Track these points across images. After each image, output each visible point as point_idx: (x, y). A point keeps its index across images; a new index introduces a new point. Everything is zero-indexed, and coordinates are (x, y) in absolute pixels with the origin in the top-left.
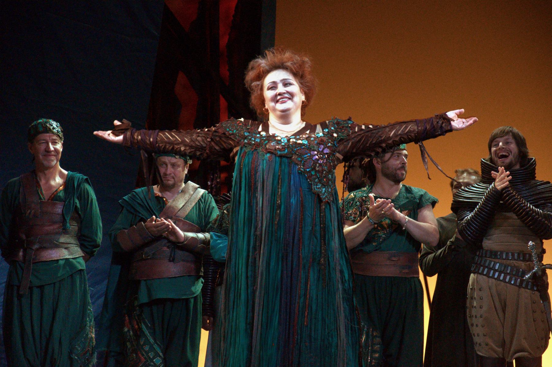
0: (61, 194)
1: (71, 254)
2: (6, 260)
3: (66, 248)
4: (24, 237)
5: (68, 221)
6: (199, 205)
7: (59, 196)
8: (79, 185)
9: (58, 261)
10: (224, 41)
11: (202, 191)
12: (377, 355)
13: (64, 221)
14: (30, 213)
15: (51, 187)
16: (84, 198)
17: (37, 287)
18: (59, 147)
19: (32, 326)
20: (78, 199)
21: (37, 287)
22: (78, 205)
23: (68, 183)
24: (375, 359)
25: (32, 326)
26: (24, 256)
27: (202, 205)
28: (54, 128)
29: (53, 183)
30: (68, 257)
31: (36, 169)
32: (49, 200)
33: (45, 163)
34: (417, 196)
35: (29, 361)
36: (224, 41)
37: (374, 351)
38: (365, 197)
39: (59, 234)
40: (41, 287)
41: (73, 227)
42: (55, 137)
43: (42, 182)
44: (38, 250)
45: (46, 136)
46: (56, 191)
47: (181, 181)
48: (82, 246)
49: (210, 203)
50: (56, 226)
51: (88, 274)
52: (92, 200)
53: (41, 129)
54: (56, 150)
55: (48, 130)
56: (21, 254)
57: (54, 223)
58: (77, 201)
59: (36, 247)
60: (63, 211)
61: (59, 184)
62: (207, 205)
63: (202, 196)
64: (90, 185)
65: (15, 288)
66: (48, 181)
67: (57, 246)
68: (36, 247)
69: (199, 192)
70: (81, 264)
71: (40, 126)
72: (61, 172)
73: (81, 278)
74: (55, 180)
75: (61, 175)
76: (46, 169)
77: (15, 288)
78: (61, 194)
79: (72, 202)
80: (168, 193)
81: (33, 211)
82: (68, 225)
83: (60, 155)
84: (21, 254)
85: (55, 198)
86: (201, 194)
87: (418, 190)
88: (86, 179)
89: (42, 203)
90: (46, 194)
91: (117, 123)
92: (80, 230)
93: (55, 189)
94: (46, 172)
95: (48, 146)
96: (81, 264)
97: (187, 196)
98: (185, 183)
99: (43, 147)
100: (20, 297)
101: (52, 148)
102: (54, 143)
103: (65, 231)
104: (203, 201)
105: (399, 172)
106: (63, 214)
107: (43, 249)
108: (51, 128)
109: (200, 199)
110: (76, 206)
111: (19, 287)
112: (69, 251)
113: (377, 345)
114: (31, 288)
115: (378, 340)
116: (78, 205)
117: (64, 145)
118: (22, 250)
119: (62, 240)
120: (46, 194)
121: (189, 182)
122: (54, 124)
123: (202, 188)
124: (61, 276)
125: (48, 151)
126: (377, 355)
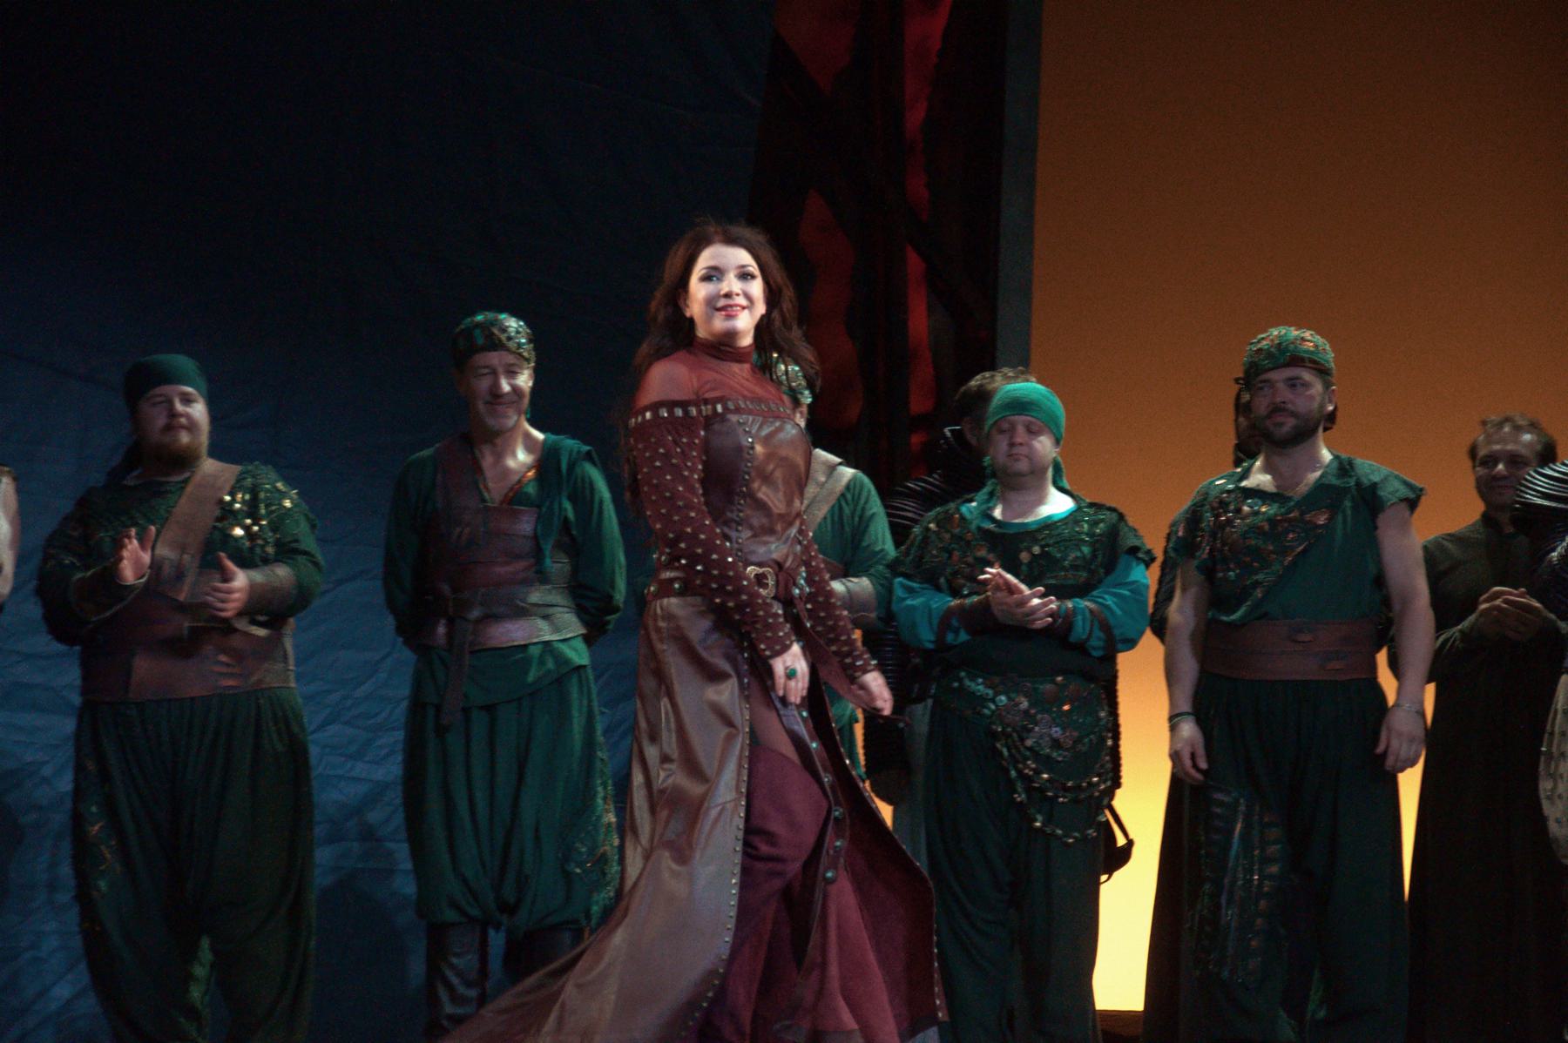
0: (531, 489)
1: (557, 630)
2: (407, 642)
3: (546, 617)
4: (446, 588)
5: (547, 553)
6: (841, 508)
7: (527, 494)
8: (572, 466)
9: (525, 646)
10: (915, 117)
11: (848, 472)
12: (1274, 869)
13: (538, 553)
14: (459, 536)
15: (507, 472)
16: (583, 497)
17: (482, 708)
18: (525, 380)
19: (473, 813)
20: (570, 498)
21: (482, 708)
22: (571, 515)
23: (547, 461)
24: (1271, 877)
25: (473, 813)
26: (450, 635)
27: (847, 510)
28: (510, 338)
29: (511, 463)
30: (547, 638)
31: (474, 435)
32: (502, 502)
33: (491, 422)
35: (465, 881)
36: (915, 117)
37: (1266, 860)
38: (1229, 492)
39: (527, 582)
40: (490, 709)
41: (557, 565)
42: (511, 359)
43: (487, 461)
44: (479, 621)
45: (494, 358)
46: (519, 481)
48: (581, 611)
49: (866, 502)
50: (521, 564)
51: (597, 678)
52: (601, 502)
53: (480, 341)
54: (516, 390)
55: (495, 344)
56: (441, 630)
57: (518, 557)
58: (568, 505)
59: (476, 613)
60: (535, 530)
61: (524, 464)
62: (858, 512)
63: (848, 487)
64: (594, 464)
65: (431, 712)
66: (499, 457)
67: (522, 612)
68: (476, 613)
69: (841, 475)
70: (579, 654)
71: (477, 332)
72: (528, 436)
73: (580, 681)
74: (514, 455)
75: (530, 444)
76: (497, 439)
77: (431, 712)
78: (531, 489)
79: (556, 506)
81: (467, 530)
82: (548, 561)
83: (526, 401)
84: (441, 630)
85: (515, 498)
86: (845, 481)
87: (1371, 468)
88: (588, 453)
89: (487, 509)
90: (495, 491)
91: (1110, 743)
92: (575, 572)
93: (516, 478)
94: (498, 441)
95: (496, 385)
96: (579, 654)
99: (484, 384)
100: (441, 731)
101: (506, 387)
102: (512, 373)
103: (542, 577)
104: (849, 496)
105: (1268, 422)
106: (535, 538)
107: (491, 618)
108: (503, 337)
109: (843, 495)
110: (566, 519)
111: (438, 708)
112: (552, 624)
113: (1274, 843)
114: (466, 711)
115: (1274, 833)
116: (571, 515)
117: (538, 375)
118: (443, 621)
119: (535, 597)
120: (495, 491)
122: (513, 324)
123: (849, 465)
124: (534, 683)
125: (495, 395)
126: (1274, 869)
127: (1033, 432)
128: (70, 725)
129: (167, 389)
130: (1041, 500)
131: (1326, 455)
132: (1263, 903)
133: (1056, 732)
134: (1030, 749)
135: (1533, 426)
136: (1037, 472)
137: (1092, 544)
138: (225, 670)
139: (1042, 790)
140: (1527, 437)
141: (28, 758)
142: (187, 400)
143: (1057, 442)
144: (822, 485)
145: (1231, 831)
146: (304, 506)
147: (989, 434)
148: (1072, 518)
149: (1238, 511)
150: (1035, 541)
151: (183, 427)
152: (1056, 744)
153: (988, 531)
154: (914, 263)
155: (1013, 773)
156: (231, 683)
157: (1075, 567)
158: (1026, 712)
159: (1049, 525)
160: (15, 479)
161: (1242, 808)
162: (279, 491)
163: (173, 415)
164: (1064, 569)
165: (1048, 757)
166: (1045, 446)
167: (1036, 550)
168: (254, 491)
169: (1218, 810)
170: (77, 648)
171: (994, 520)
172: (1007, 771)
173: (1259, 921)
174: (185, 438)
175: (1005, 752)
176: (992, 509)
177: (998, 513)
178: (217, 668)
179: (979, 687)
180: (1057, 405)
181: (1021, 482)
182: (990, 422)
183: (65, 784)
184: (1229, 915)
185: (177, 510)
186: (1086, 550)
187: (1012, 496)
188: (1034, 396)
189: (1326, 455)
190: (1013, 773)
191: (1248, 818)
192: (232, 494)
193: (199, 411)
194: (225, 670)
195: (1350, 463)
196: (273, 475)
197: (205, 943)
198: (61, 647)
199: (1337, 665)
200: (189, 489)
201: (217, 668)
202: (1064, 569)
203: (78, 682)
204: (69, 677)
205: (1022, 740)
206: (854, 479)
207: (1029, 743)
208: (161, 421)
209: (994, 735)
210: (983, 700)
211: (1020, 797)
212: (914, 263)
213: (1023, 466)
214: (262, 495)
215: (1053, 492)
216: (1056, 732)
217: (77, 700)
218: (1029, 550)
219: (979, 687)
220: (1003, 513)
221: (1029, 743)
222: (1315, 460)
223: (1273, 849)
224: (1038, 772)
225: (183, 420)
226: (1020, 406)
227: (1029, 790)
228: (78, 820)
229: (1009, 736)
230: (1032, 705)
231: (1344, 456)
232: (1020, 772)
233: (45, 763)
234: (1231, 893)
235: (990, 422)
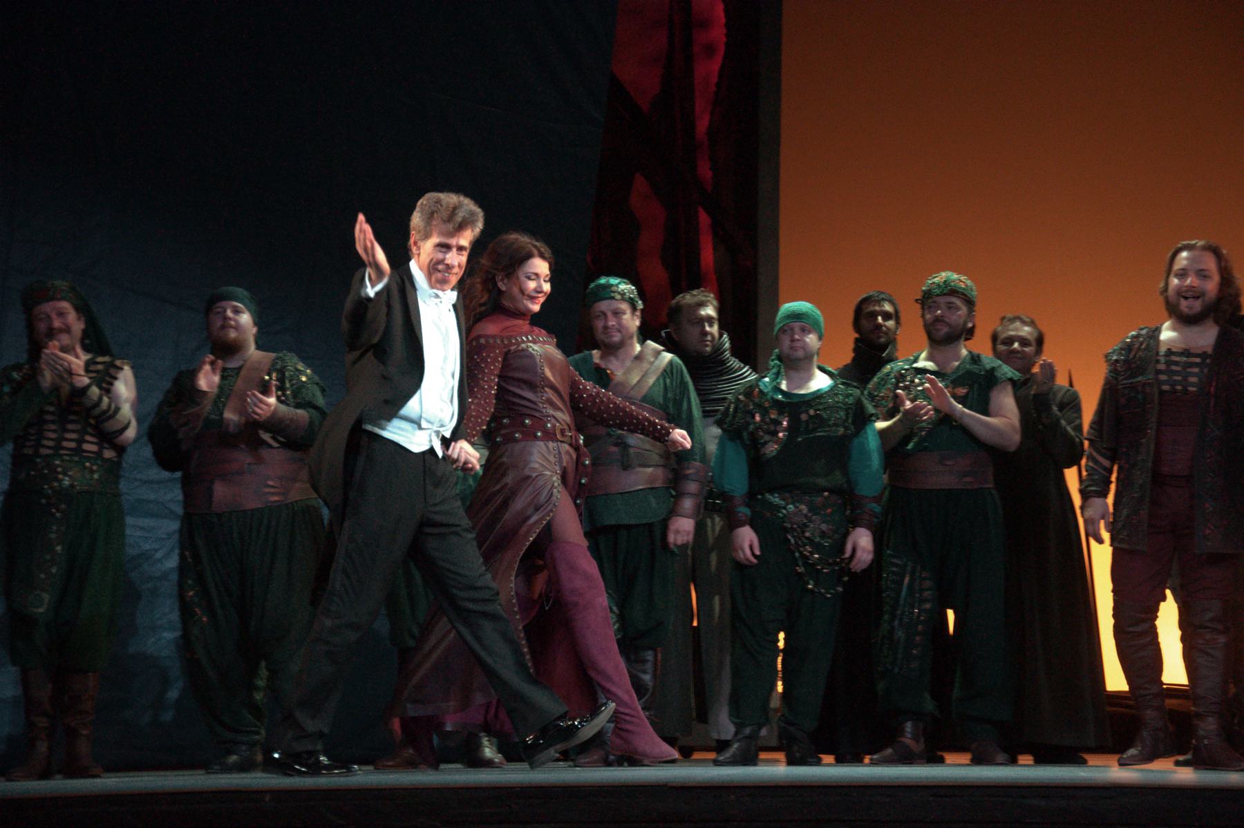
10: (702, 124)
11: (668, 356)
12: (928, 606)
34: (988, 367)
36: (702, 124)
47: (631, 337)
80: (613, 359)
97: (645, 365)
98: (642, 342)
121: (650, 342)
123: (669, 351)
127: (804, 331)
128: (175, 525)
129: (223, 304)
130: (810, 377)
131: (964, 352)
132: (920, 627)
133: (824, 527)
134: (807, 538)
135: (1032, 323)
136: (808, 357)
137: (846, 410)
138: (272, 490)
139: (813, 565)
140: (1026, 328)
141: (147, 546)
142: (237, 311)
143: (820, 338)
144: (652, 363)
145: (902, 581)
146: (317, 378)
147: (777, 337)
148: (832, 391)
149: (912, 381)
150: (811, 407)
151: (231, 327)
152: (823, 534)
153: (778, 401)
154: (704, 219)
155: (797, 554)
156: (276, 498)
157: (836, 425)
158: (806, 516)
159: (818, 396)
160: (132, 368)
161: (909, 568)
162: (298, 370)
163: (226, 318)
164: (829, 426)
165: (819, 544)
166: (812, 339)
167: (812, 412)
168: (281, 372)
169: (51, 409)
170: (178, 474)
171: (782, 392)
172: (793, 553)
173: (918, 638)
174: (233, 334)
175: (793, 541)
176: (779, 384)
177: (784, 386)
178: (267, 490)
179: (776, 499)
180: (817, 313)
181: (796, 364)
182: (776, 329)
183: (173, 562)
184: (900, 634)
185: (236, 388)
186: (842, 414)
187: (792, 373)
188: (804, 310)
189: (964, 352)
190: (797, 554)
191: (913, 574)
192: (269, 374)
193: (246, 318)
194: (272, 490)
195: (978, 356)
196: (295, 359)
197: (263, 664)
198: (166, 474)
199: (968, 479)
200: (243, 373)
201: (267, 490)
202: (829, 426)
203: (181, 497)
204: (174, 496)
205: (803, 532)
206: (671, 363)
207: (807, 534)
208: (219, 324)
209: (786, 530)
210: (778, 508)
211: (800, 570)
212: (704, 219)
213: (800, 354)
214: (287, 374)
215: (818, 373)
216: (824, 527)
217: (180, 510)
218: (807, 412)
219: (776, 499)
220: (788, 385)
221: (807, 534)
222: (957, 356)
223: (927, 594)
224: (812, 553)
225: (233, 323)
226: (797, 316)
227: (806, 564)
228: (181, 587)
229: (795, 530)
230: (810, 510)
231: (976, 352)
232: (801, 553)
233: (156, 550)
234: (901, 620)
235: (776, 329)
